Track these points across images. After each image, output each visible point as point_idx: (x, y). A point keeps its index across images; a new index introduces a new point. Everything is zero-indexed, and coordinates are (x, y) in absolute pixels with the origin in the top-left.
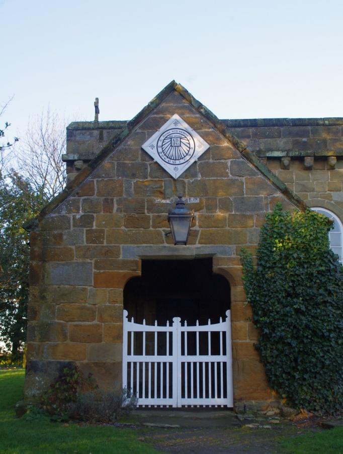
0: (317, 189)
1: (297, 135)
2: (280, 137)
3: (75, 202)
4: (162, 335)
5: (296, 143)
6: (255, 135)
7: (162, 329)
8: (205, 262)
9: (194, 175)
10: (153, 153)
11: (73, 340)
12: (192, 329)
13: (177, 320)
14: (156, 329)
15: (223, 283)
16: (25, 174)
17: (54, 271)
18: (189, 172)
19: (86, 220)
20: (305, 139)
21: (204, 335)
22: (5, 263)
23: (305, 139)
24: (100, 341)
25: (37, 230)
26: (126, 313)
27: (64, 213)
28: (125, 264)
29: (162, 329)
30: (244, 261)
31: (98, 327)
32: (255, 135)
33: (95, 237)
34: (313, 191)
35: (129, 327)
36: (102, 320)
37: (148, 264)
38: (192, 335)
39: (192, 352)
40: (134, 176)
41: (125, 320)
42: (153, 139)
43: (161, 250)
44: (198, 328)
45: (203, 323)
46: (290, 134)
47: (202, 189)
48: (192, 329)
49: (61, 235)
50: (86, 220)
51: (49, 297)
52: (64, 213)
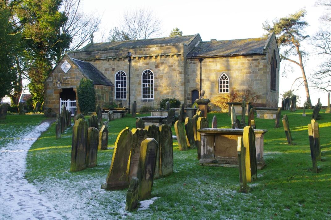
0: (120, 65)
1: (116, 52)
2: (112, 53)
3: (50, 78)
4: (66, 103)
5: (115, 54)
6: (107, 53)
7: (66, 102)
8: (72, 89)
9: (69, 72)
10: (62, 68)
11: (51, 104)
12: (71, 101)
13: (69, 100)
14: (66, 101)
15: (74, 93)
16: (126, 31)
17: (48, 91)
18: (68, 72)
19: (52, 82)
20: (117, 53)
21: (73, 102)
22: (77, 80)
23: (117, 53)
24: (55, 104)
25: (45, 83)
26: (61, 99)
27: (49, 80)
28: (59, 90)
29: (66, 102)
30: (77, 89)
31: (55, 101)
32: (107, 53)
33: (54, 85)
34: (120, 66)
35: (61, 101)
36: (55, 100)
37: (64, 89)
38: (71, 102)
39: (71, 106)
40: (60, 73)
41: (61, 100)
42: (62, 65)
43: (64, 87)
44: (72, 101)
45: (73, 100)
46: (114, 52)
47: (70, 75)
48: (71, 101)
49: (48, 85)
50: (52, 82)
51: (47, 96)
52: (49, 80)
